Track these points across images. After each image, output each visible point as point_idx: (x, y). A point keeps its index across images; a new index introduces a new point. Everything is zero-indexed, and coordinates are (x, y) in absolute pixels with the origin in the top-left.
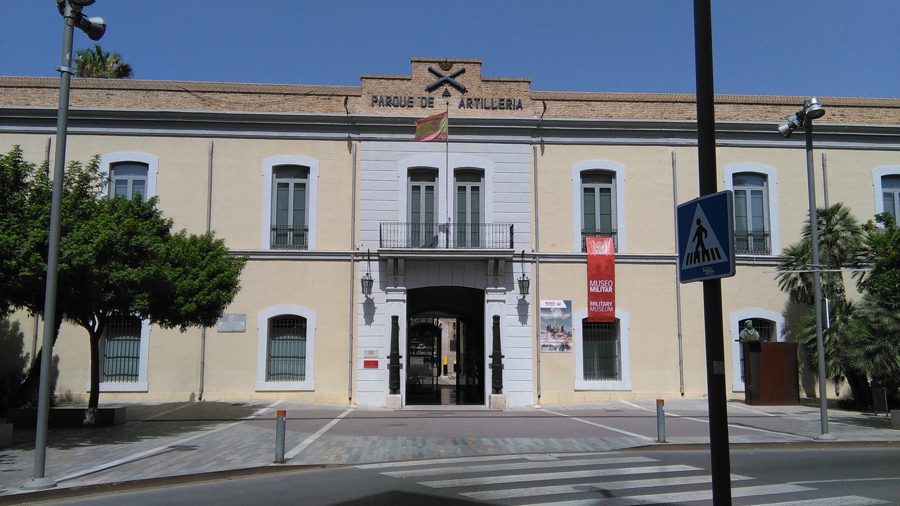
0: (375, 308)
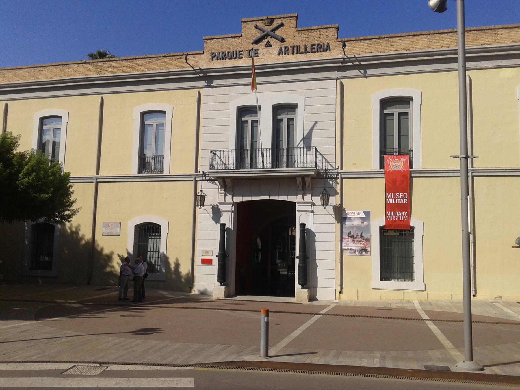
0: (213, 219)
